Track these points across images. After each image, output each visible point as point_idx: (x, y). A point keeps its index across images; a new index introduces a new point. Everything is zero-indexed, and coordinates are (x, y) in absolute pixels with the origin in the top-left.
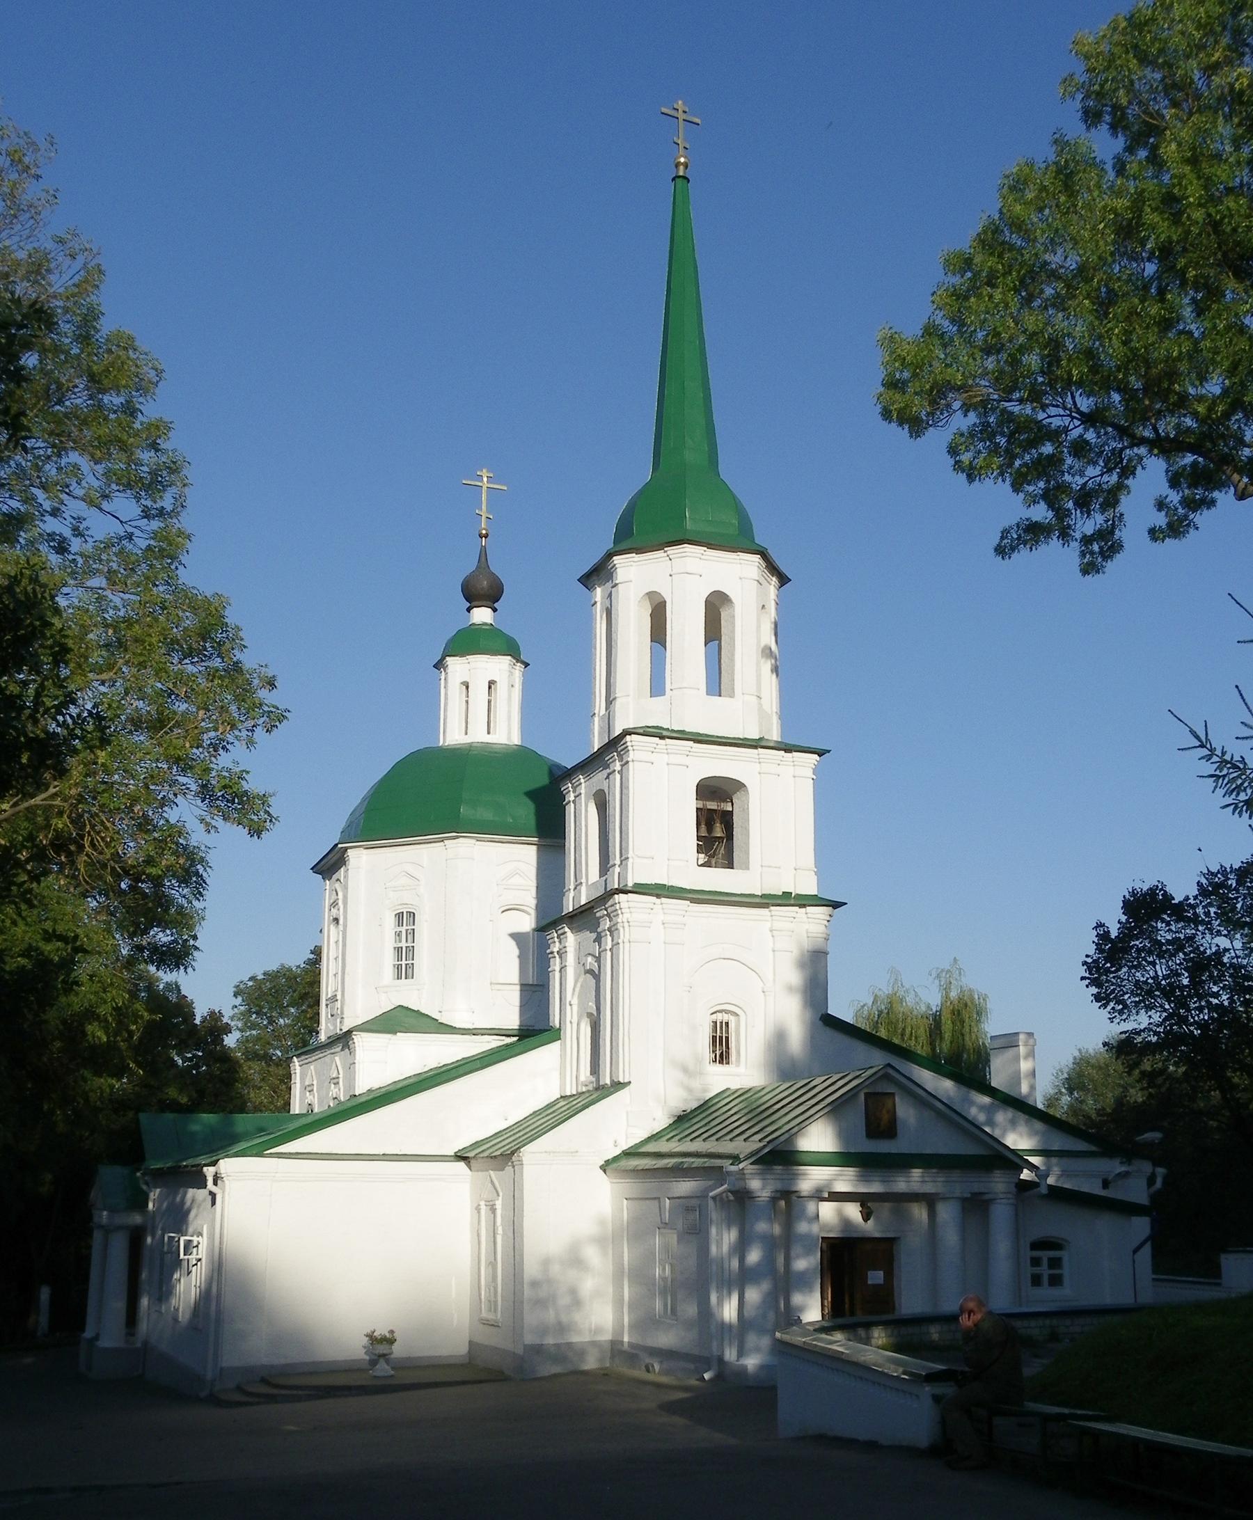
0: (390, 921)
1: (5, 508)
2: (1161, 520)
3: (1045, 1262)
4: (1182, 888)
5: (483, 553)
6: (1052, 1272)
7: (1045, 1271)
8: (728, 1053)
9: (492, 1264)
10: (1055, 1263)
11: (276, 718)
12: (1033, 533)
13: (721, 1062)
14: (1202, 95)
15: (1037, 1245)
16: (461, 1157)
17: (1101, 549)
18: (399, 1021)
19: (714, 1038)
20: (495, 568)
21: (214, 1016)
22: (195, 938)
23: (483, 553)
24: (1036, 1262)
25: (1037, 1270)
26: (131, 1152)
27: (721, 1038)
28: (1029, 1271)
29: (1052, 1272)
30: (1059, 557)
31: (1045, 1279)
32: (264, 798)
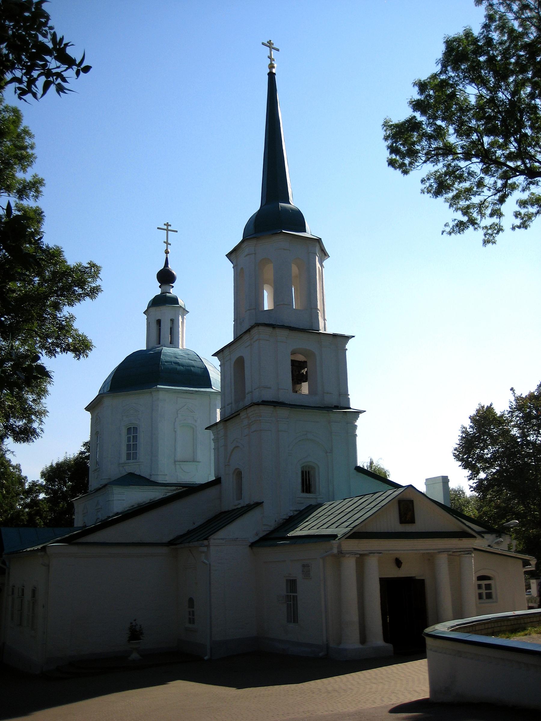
0: (124, 431)
2: (518, 222)
3: (484, 586)
4: (403, 113)
6: (487, 591)
7: (484, 591)
9: (438, 633)
10: (488, 587)
11: (94, 292)
12: (461, 226)
13: (307, 492)
15: (480, 578)
17: (491, 235)
18: (133, 480)
22: (24, 442)
24: (480, 587)
25: (480, 591)
26: (494, 416)
27: (306, 479)
29: (487, 591)
30: (472, 236)
31: (484, 596)
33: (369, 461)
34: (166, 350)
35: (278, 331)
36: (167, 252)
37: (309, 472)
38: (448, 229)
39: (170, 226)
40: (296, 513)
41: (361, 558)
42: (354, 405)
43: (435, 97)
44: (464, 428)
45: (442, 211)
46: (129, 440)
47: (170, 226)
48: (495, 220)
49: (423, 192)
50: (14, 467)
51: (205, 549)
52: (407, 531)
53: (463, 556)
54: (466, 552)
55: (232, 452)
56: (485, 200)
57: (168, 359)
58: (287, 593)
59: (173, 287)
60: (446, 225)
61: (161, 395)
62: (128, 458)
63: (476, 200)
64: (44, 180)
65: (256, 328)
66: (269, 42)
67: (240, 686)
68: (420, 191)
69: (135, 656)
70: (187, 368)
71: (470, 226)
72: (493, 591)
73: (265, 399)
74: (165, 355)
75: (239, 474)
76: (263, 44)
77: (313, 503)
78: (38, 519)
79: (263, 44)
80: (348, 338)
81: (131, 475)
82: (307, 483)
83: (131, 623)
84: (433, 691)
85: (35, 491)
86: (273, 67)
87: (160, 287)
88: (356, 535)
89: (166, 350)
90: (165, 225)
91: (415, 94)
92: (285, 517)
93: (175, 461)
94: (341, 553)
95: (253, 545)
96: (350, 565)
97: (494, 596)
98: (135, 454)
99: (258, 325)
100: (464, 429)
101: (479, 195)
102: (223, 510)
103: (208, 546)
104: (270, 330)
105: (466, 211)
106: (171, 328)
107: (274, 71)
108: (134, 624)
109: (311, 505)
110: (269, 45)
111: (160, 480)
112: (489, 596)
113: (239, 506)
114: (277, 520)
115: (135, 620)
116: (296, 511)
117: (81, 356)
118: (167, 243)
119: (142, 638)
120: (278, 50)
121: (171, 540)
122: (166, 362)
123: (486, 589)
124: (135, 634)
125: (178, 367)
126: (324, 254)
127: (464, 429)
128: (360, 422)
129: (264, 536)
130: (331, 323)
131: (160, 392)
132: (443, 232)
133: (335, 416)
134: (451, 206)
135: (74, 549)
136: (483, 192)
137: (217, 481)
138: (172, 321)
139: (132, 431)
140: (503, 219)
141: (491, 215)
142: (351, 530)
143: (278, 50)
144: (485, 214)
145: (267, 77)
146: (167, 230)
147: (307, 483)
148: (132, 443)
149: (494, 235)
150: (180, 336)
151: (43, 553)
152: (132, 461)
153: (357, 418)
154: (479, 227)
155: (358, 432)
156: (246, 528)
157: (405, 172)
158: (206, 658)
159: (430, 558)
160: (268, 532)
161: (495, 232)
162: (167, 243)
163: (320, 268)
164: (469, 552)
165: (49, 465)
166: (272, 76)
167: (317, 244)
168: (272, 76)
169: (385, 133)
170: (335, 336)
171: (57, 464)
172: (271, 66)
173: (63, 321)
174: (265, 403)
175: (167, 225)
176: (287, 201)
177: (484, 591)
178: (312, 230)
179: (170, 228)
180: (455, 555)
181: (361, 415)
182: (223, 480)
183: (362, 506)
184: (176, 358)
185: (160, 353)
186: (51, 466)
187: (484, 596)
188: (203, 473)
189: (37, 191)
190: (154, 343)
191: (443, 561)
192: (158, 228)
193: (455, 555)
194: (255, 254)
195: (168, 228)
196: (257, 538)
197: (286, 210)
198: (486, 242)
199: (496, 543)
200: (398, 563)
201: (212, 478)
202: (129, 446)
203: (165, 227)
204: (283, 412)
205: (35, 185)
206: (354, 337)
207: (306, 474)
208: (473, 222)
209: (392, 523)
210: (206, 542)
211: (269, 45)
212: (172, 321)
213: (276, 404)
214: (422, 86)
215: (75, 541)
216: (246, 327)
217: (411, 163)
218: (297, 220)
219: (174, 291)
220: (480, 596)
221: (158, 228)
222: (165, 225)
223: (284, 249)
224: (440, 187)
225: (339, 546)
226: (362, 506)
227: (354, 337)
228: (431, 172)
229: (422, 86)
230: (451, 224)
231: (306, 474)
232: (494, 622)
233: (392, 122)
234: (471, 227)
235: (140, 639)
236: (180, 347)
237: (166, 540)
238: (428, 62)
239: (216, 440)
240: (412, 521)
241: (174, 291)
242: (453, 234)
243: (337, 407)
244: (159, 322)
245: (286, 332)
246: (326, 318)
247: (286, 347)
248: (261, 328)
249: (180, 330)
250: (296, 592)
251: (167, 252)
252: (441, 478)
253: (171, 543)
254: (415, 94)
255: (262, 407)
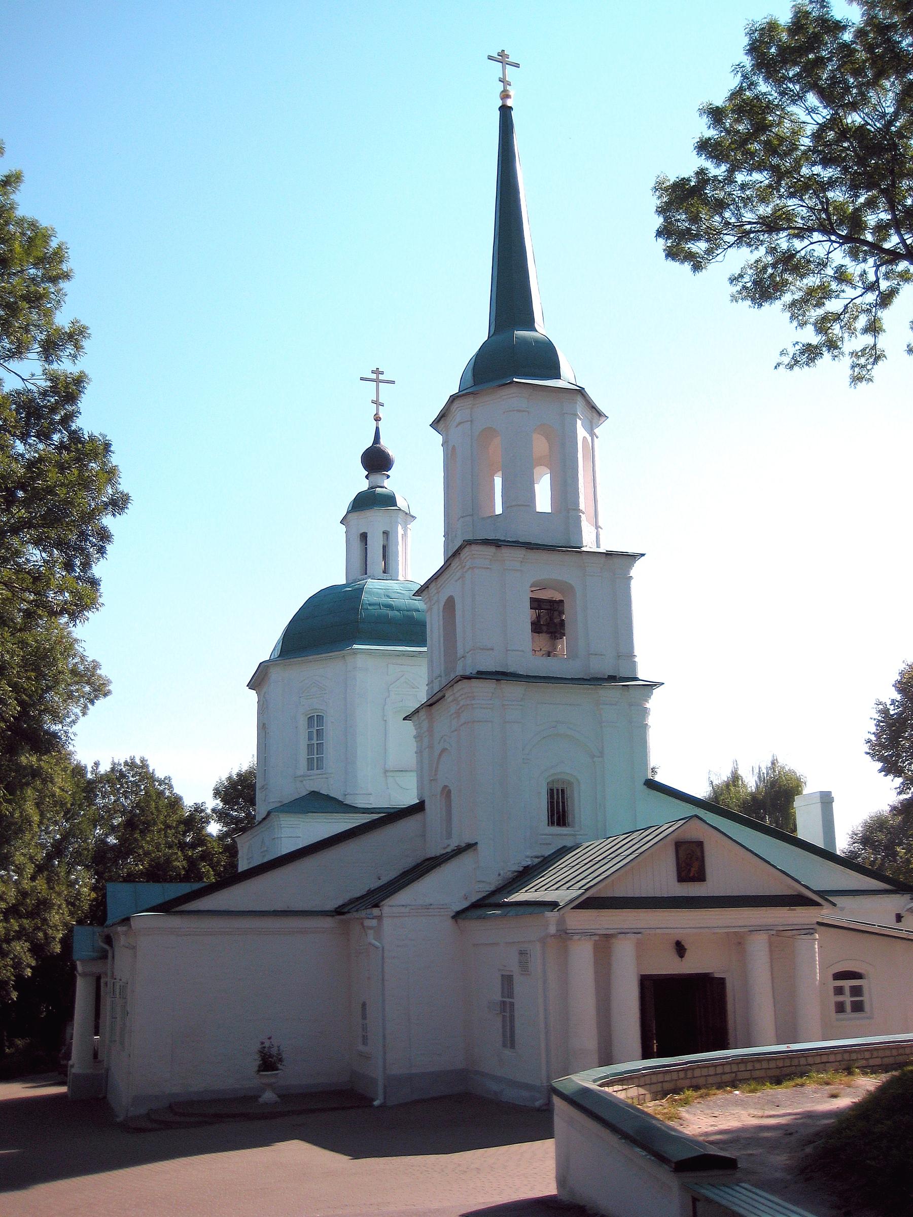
0: (303, 722)
1: (12, 384)
3: (847, 991)
4: (687, 165)
5: (377, 429)
7: (847, 999)
8: (564, 815)
10: (857, 991)
12: (811, 353)
13: (559, 824)
14: (55, 414)
15: (839, 976)
16: (512, 357)
18: (317, 802)
19: (552, 803)
20: (386, 443)
21: (198, 809)
23: (377, 429)
24: (839, 991)
25: (840, 998)
27: (558, 803)
28: (834, 999)
30: (832, 369)
31: (848, 1007)
32: (114, 764)
33: (770, 759)
34: (372, 585)
35: (506, 552)
36: (377, 419)
37: (563, 791)
38: (786, 360)
39: (382, 373)
40: (537, 861)
41: (604, 944)
42: (644, 673)
43: (742, 129)
44: (881, 703)
45: (776, 325)
46: (310, 739)
47: (382, 373)
48: (868, 339)
49: (734, 299)
50: (161, 783)
51: (374, 922)
52: (690, 895)
53: (799, 937)
54: (804, 932)
55: (440, 755)
56: (846, 307)
57: (374, 599)
58: (503, 997)
59: (388, 477)
60: (782, 353)
61: (360, 661)
62: (310, 767)
63: (834, 306)
64: (87, 328)
65: (466, 549)
66: (502, 54)
67: (356, 1153)
68: (730, 298)
69: (269, 1096)
70: (406, 613)
71: (825, 353)
72: (865, 998)
73: (483, 668)
74: (370, 593)
75: (447, 793)
76: (490, 58)
77: (569, 845)
78: (204, 866)
79: (490, 58)
80: (633, 557)
81: (315, 795)
82: (559, 812)
83: (262, 1043)
84: (562, 1181)
85: (201, 820)
86: (508, 96)
87: (367, 477)
88: (590, 903)
89: (372, 585)
90: (373, 372)
91: (706, 130)
92: (516, 868)
93: (386, 771)
94: (564, 935)
95: (458, 915)
96: (582, 955)
97: (867, 1006)
98: (320, 760)
99: (468, 543)
100: (881, 707)
101: (837, 297)
102: (428, 856)
103: (379, 918)
104: (492, 550)
105: (822, 325)
106: (384, 547)
107: (509, 103)
108: (267, 1045)
109: (564, 847)
110: (502, 58)
111: (361, 802)
112: (858, 1007)
113: (449, 850)
114: (502, 872)
115: (270, 1038)
116: (538, 857)
117: (78, 621)
118: (377, 403)
119: (280, 1067)
120: (517, 65)
121: (340, 907)
122: (370, 605)
123: (852, 995)
124: (269, 1062)
125: (391, 613)
126: (595, 413)
127: (881, 707)
128: (655, 703)
129: (478, 900)
130: (599, 534)
131: (358, 656)
132: (779, 364)
133: (608, 693)
134: (793, 317)
135: (174, 921)
136: (843, 291)
137: (419, 807)
138: (386, 533)
139: (316, 721)
140: (882, 338)
141: (866, 330)
142: (583, 893)
143: (517, 65)
144: (855, 329)
145: (497, 114)
146: (378, 381)
147: (559, 812)
148: (315, 742)
149: (869, 367)
150: (400, 559)
151: (125, 928)
152: (315, 771)
153: (647, 697)
154: (843, 354)
155: (651, 720)
156: (448, 887)
157: (697, 267)
158: (376, 1103)
159: (737, 942)
160: (484, 894)
161: (871, 360)
162: (377, 403)
163: (589, 439)
164: (809, 931)
165: (224, 777)
166: (505, 112)
167: (579, 399)
168: (505, 112)
169: (658, 202)
170: (609, 554)
171: (239, 775)
172: (505, 95)
173: (41, 566)
174: (482, 675)
175: (377, 372)
176: (529, 324)
177: (847, 999)
178: (570, 372)
179: (381, 377)
180: (781, 939)
181: (656, 692)
182: (427, 805)
183: (619, 851)
184: (388, 596)
185: (361, 590)
186: (230, 778)
187: (848, 1007)
188: (405, 794)
189: (78, 347)
190: (357, 573)
191: (759, 947)
192: (362, 379)
193: (781, 939)
194: (471, 421)
195: (378, 377)
196: (466, 904)
197: (525, 342)
198: (857, 379)
199: (908, 910)
200: (680, 949)
201: (411, 799)
202: (310, 747)
203: (374, 376)
204: (513, 690)
205: (75, 337)
206: (643, 555)
207: (558, 794)
208: (832, 345)
209: (663, 879)
210: (376, 911)
211: (502, 58)
212: (386, 533)
213: (501, 676)
214: (716, 115)
215: (177, 909)
216: (458, 544)
217: (709, 252)
218: (544, 360)
219: (392, 483)
220: (840, 1008)
221: (362, 379)
222: (373, 372)
223: (518, 411)
224: (762, 289)
225: (561, 922)
226: (619, 851)
227: (643, 555)
228: (750, 263)
229: (716, 115)
230: (792, 351)
231: (558, 794)
232: (738, 1064)
233: (669, 180)
234: (827, 356)
235: (277, 1070)
236: (401, 578)
237: (331, 905)
238: (721, 70)
239: (418, 737)
240: (700, 877)
241: (392, 483)
242: (796, 368)
243: (612, 678)
244: (364, 537)
245: (520, 553)
246: (600, 524)
247: (522, 578)
248: (474, 548)
249: (400, 548)
250: (512, 997)
251: (377, 419)
252: (818, 794)
253: (339, 912)
254: (706, 130)
255: (474, 683)
